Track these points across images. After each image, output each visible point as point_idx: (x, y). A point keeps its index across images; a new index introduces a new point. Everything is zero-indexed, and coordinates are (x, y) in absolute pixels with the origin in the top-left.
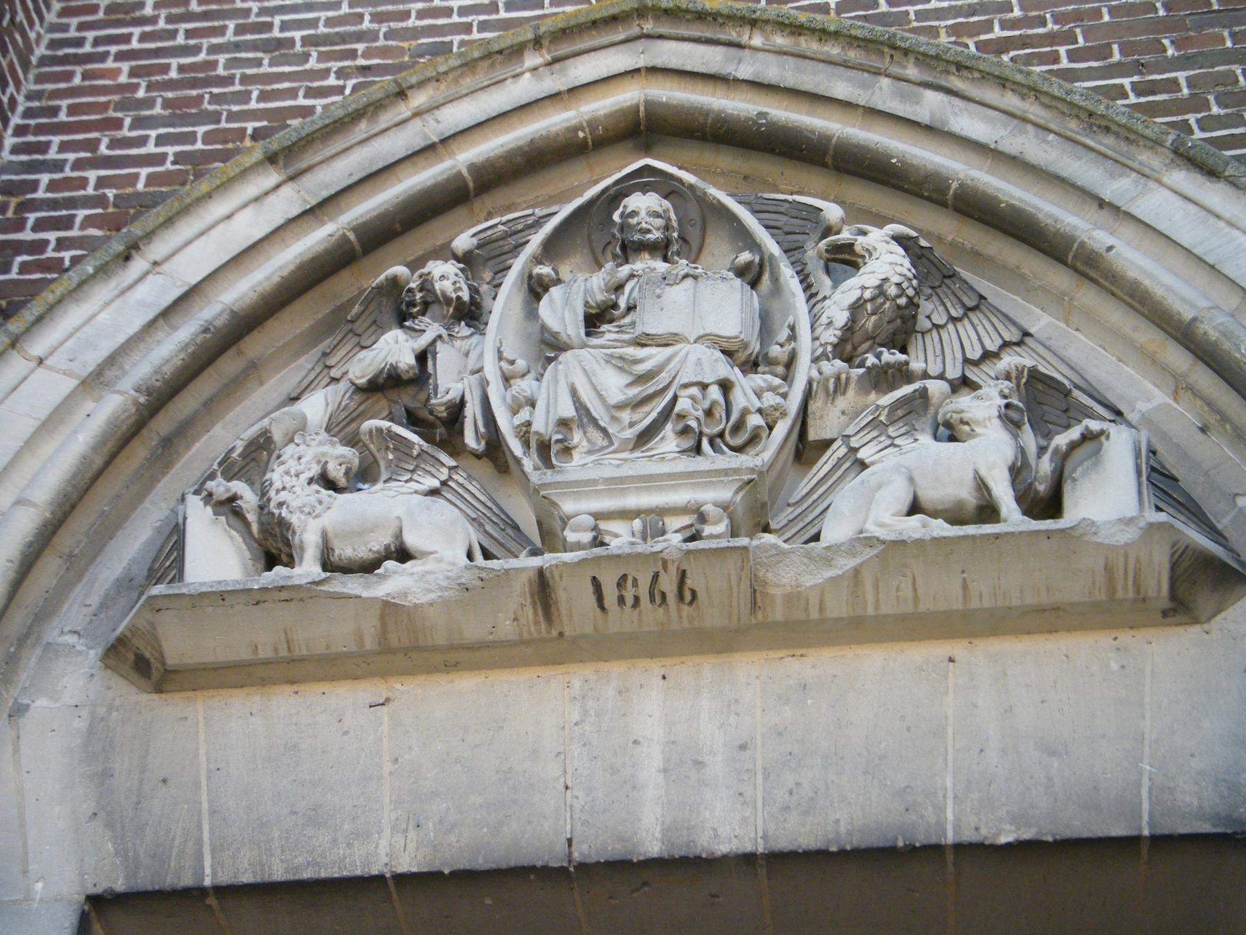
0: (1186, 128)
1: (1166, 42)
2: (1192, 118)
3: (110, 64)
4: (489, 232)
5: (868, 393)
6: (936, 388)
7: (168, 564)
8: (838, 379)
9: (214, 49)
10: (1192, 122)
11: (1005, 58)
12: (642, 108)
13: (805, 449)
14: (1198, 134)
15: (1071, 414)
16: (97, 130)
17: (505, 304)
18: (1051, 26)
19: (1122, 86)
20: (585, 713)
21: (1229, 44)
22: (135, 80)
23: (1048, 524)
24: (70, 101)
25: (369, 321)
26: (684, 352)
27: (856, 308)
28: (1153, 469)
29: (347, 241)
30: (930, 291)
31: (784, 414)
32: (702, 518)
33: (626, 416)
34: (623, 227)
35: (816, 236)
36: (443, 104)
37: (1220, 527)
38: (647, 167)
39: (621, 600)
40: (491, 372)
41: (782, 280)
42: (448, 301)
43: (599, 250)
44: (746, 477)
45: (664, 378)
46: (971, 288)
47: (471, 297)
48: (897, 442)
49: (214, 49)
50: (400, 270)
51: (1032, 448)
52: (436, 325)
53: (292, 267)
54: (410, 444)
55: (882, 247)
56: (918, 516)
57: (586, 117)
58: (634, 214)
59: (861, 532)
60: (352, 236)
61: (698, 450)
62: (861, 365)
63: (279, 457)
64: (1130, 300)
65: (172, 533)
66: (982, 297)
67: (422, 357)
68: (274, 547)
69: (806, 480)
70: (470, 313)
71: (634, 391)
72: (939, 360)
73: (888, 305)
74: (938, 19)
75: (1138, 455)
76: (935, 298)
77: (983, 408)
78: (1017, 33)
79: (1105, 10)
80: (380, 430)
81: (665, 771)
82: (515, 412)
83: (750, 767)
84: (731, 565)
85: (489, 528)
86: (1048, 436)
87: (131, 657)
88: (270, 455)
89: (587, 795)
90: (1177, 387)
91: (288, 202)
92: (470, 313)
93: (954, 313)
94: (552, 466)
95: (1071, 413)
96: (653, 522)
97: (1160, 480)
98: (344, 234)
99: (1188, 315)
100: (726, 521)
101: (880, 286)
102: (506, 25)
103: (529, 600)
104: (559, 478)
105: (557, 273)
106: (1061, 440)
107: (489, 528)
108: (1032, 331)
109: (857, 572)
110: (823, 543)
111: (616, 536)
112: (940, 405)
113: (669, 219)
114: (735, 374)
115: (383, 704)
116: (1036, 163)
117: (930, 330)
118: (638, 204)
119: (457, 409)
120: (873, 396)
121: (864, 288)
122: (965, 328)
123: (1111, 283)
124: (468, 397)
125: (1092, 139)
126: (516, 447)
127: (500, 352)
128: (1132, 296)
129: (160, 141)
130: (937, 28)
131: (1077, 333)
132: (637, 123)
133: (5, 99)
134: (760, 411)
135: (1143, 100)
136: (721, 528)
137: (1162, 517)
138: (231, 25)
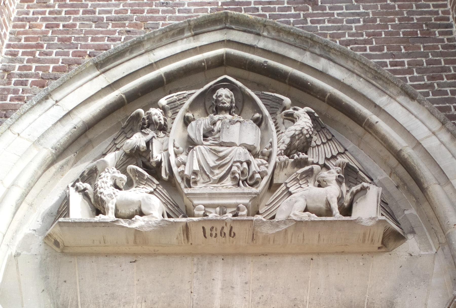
0: (405, 80)
1: (402, 47)
2: (408, 76)
4: (171, 99)
5: (294, 168)
6: (316, 167)
7: (64, 210)
8: (285, 163)
9: (75, 19)
10: (408, 78)
11: (349, 48)
12: (225, 56)
13: (272, 186)
14: (409, 83)
15: (358, 180)
16: (34, 48)
17: (176, 127)
18: (365, 37)
19: (386, 62)
20: (198, 269)
21: (422, 50)
22: (48, 29)
23: (347, 218)
24: (25, 36)
25: (130, 128)
26: (235, 150)
28: (382, 201)
29: (123, 98)
30: (316, 132)
31: (267, 174)
32: (238, 209)
33: (216, 171)
34: (217, 101)
35: (281, 110)
36: (156, 48)
37: (398, 220)
38: (225, 80)
39: (211, 235)
40: (171, 151)
41: (269, 125)
42: (157, 123)
43: (208, 107)
44: (254, 196)
46: (330, 132)
47: (165, 123)
48: (302, 186)
49: (75, 19)
51: (344, 192)
52: (153, 132)
53: (103, 107)
54: (144, 175)
55: (302, 115)
56: (307, 213)
57: (205, 58)
58: (220, 96)
59: (289, 217)
60: (124, 96)
61: (238, 185)
62: (293, 158)
63: (100, 176)
64: (381, 141)
65: (65, 199)
66: (333, 136)
67: (148, 143)
68: (98, 208)
69: (272, 197)
70: (163, 128)
71: (218, 163)
72: (317, 157)
73: (303, 137)
74: (327, 30)
75: (378, 196)
76: (318, 135)
77: (331, 175)
78: (353, 38)
79: (383, 33)
80: (134, 169)
81: (222, 289)
82: (178, 167)
83: (248, 289)
84: (247, 226)
85: (169, 206)
86: (350, 187)
87: (53, 241)
88: (97, 175)
89: (198, 295)
90: (391, 172)
91: (102, 81)
92: (163, 128)
93: (324, 141)
95: (359, 180)
96: (223, 209)
97: (384, 205)
98: (121, 96)
99: (399, 148)
100: (246, 210)
101: (301, 130)
102: (178, 18)
103: (182, 232)
104: (193, 192)
105: (193, 116)
106: (354, 189)
107: (169, 206)
108: (347, 149)
109: (286, 230)
110: (276, 220)
111: (211, 213)
112: (317, 174)
113: (232, 99)
114: (251, 158)
115: (134, 262)
116: (356, 88)
117: (315, 147)
118: (222, 93)
119: (159, 164)
120: (296, 169)
121: (296, 130)
122: (327, 147)
123: (376, 135)
124: (163, 160)
125: (375, 81)
126: (179, 179)
127: (174, 144)
128: (382, 140)
129: (57, 54)
130: (327, 33)
131: (362, 151)
132: (222, 61)
133: (2, 33)
134: (259, 173)
135: (393, 68)
136: (245, 212)
137: (384, 218)
138: (81, 10)
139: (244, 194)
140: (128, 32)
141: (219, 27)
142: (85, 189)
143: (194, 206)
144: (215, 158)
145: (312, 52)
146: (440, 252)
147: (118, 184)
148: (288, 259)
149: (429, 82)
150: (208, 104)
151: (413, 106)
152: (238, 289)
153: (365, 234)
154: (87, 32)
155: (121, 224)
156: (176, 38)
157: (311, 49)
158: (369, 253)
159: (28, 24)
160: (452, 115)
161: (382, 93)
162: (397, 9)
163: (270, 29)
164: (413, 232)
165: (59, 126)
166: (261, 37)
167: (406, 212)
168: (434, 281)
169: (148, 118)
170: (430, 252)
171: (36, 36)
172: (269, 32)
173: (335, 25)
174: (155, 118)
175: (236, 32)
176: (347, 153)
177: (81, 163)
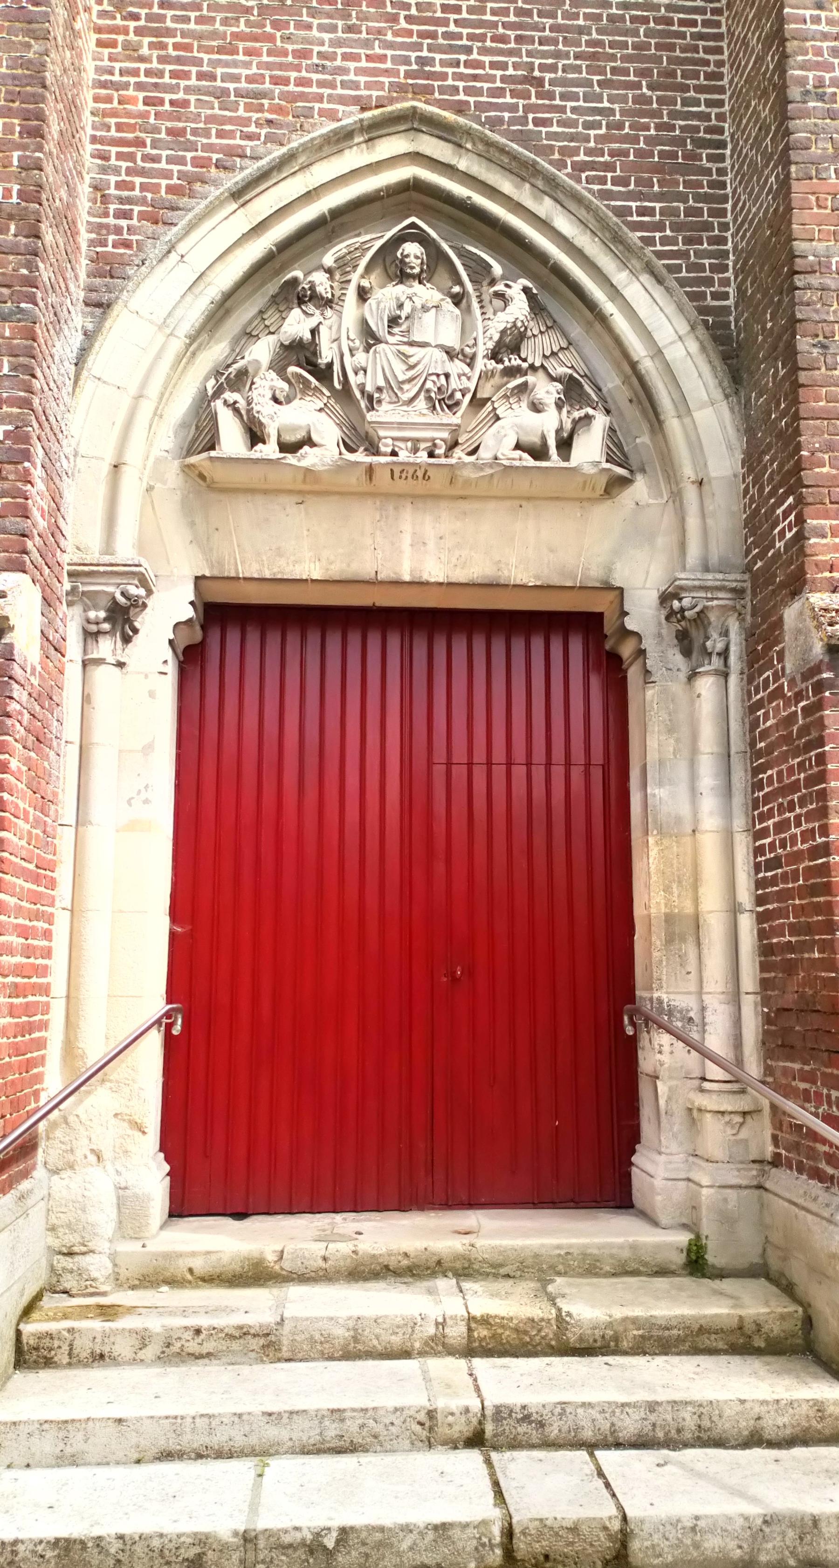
1: (655, 180)
3: (131, 92)
20: (381, 516)
23: (565, 464)
27: (503, 332)
31: (469, 391)
32: (435, 445)
34: (402, 261)
38: (413, 225)
42: (322, 298)
43: (388, 264)
45: (420, 368)
50: (298, 274)
58: (407, 256)
60: (274, 248)
66: (555, 321)
67: (314, 332)
77: (547, 391)
94: (373, 409)
99: (636, 359)
109: (492, 475)
119: (330, 365)
126: (358, 395)
139: (442, 425)
140: (270, 122)
141: (403, 128)
142: (235, 402)
143: (380, 439)
144: (405, 367)
145: (533, 185)
146: (671, 503)
147: (278, 396)
148: (492, 505)
149: (684, 248)
150: (389, 260)
151: (658, 292)
152: (431, 545)
153: (585, 483)
154: (210, 119)
155: (288, 461)
156: (340, 146)
157: (532, 180)
158: (589, 499)
159: (116, 95)
160: (707, 307)
161: (622, 265)
162: (655, 106)
163: (477, 141)
164: (643, 470)
165: (189, 298)
166: (463, 151)
167: (638, 440)
168: (660, 541)
169: (310, 289)
170: (660, 501)
171: (133, 121)
172: (474, 144)
173: (567, 130)
174: (320, 289)
175: (426, 138)
176: (571, 348)
177: (217, 343)
